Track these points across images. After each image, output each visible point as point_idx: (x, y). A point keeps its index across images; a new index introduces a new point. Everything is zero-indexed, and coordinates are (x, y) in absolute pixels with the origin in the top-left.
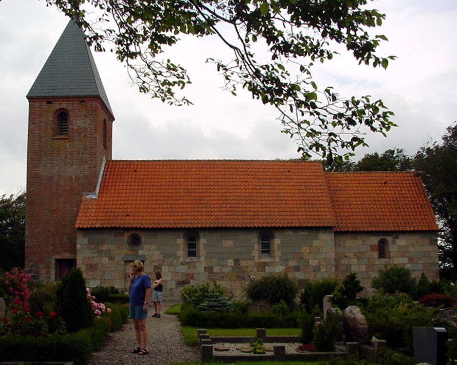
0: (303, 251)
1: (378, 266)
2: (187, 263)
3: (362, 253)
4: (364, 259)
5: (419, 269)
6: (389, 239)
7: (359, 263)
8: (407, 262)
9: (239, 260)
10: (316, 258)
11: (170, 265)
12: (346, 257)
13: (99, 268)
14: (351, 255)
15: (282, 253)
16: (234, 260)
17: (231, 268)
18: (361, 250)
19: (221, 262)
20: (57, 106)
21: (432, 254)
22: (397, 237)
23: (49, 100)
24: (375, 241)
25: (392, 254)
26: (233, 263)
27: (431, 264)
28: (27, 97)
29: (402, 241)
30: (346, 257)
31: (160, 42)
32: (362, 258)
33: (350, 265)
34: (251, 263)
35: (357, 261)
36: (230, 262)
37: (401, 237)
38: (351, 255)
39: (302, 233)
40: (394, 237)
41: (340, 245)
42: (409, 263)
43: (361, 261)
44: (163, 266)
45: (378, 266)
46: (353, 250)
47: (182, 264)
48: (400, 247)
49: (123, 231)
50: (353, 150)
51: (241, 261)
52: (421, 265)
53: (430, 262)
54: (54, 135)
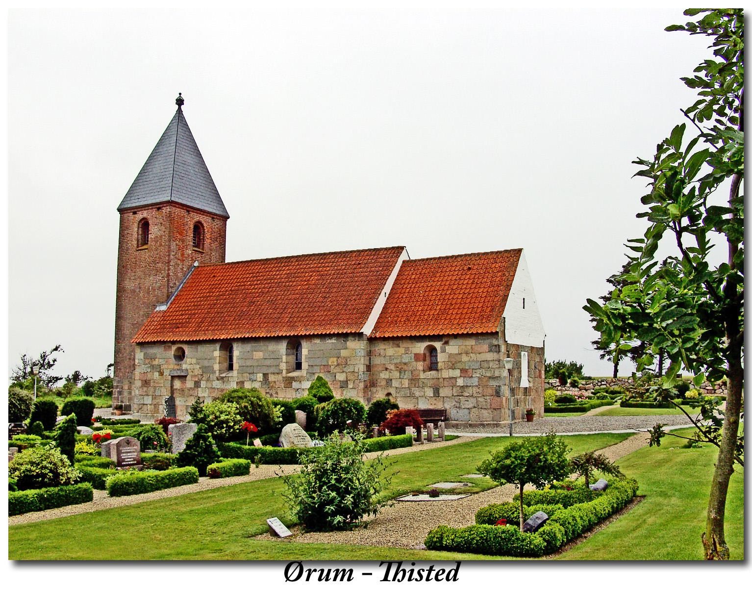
0: (330, 364)
1: (423, 380)
2: (222, 378)
3: (405, 364)
4: (406, 372)
5: (474, 385)
6: (438, 345)
7: (401, 377)
8: (459, 375)
9: (268, 374)
10: (343, 372)
11: (208, 380)
12: (386, 369)
13: (152, 384)
14: (392, 367)
15: (309, 366)
16: (264, 374)
17: (260, 383)
18: (404, 361)
19: (252, 377)
20: (140, 216)
21: (491, 364)
22: (446, 343)
23: (135, 210)
24: (420, 347)
25: (439, 365)
26: (262, 377)
27: (490, 378)
28: (119, 210)
29: (453, 347)
30: (386, 369)
31: (14, 383)
32: (405, 371)
33: (391, 380)
34: (280, 377)
35: (398, 374)
36: (260, 377)
37: (452, 342)
38: (392, 367)
39: (330, 341)
40: (443, 342)
41: (380, 354)
42: (461, 376)
43: (402, 374)
44: (202, 382)
45: (423, 380)
46: (395, 361)
47: (218, 379)
48: (450, 355)
49: (170, 345)
50: (684, 126)
51: (270, 375)
52: (477, 380)
53: (488, 375)
54: (138, 246)
